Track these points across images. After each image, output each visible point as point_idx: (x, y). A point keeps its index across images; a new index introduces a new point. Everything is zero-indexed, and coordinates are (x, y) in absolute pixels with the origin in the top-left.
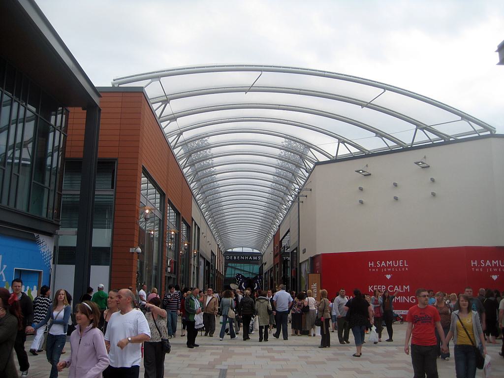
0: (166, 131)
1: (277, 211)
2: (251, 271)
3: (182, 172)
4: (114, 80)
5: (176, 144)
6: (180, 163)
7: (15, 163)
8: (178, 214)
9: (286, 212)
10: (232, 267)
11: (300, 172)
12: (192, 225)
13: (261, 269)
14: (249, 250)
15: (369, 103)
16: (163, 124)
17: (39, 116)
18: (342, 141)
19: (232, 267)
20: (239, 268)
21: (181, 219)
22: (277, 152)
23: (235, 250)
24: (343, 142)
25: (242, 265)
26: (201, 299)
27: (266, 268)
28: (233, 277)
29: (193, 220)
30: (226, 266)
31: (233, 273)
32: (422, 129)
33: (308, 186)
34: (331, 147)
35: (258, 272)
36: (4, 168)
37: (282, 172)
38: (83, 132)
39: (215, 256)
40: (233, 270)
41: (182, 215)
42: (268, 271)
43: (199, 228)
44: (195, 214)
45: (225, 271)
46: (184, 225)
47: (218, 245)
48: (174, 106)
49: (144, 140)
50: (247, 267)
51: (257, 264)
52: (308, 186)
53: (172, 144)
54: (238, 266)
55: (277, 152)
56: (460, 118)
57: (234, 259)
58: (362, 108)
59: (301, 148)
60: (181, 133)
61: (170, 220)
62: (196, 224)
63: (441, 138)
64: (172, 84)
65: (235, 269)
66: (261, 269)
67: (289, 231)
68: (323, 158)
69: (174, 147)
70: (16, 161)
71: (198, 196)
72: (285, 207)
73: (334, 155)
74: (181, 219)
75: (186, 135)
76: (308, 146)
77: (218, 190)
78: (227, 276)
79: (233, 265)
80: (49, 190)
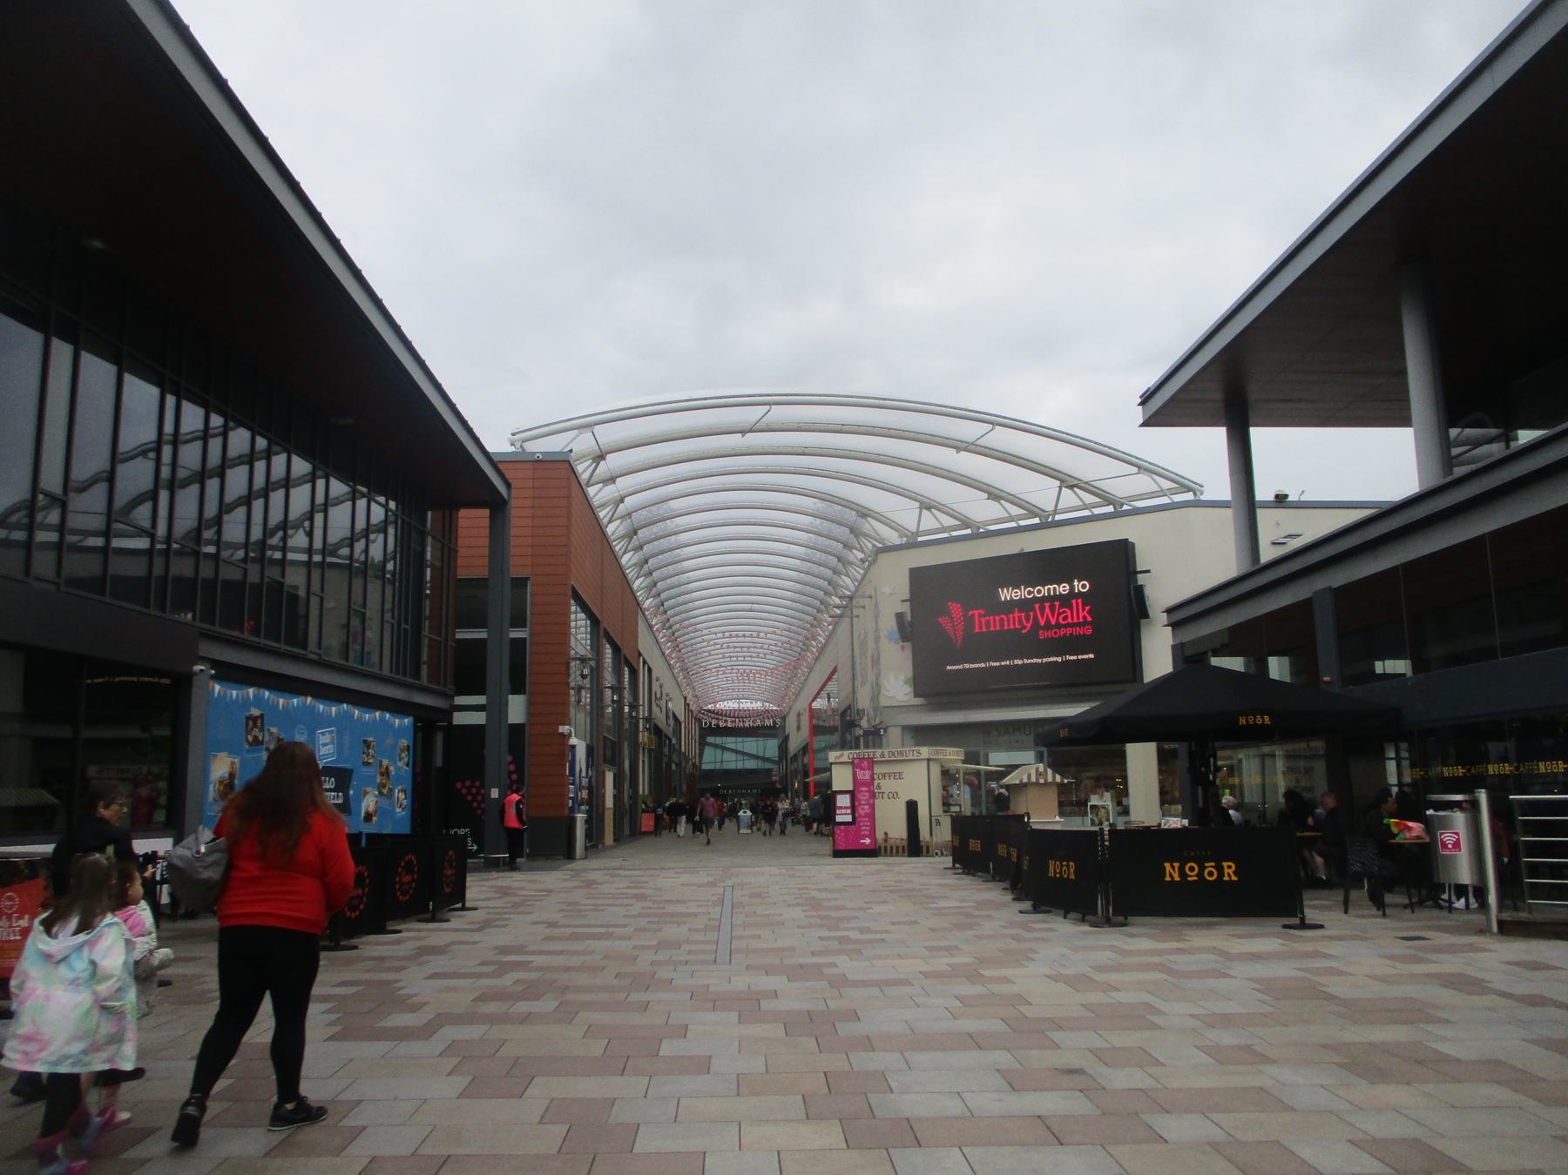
0: (596, 502)
1: (835, 572)
2: (761, 754)
3: (604, 534)
4: (513, 434)
5: (591, 476)
6: (601, 514)
7: (316, 563)
8: (595, 621)
9: (862, 572)
10: (716, 746)
11: (867, 525)
12: (639, 663)
13: (783, 747)
14: (757, 705)
15: (972, 444)
16: (591, 491)
17: (413, 522)
18: (927, 505)
19: (716, 746)
20: (733, 746)
21: (602, 633)
22: (805, 520)
23: (721, 706)
24: (929, 508)
25: (740, 739)
26: (1464, 805)
27: (794, 744)
28: (718, 767)
29: (640, 654)
30: (703, 744)
31: (719, 760)
32: (1071, 487)
33: (868, 590)
34: (907, 515)
35: (777, 754)
36: (363, 611)
37: (818, 556)
38: (486, 552)
39: (680, 724)
40: (719, 752)
41: (604, 624)
42: (799, 751)
43: (650, 670)
44: (645, 643)
45: (701, 756)
46: (608, 646)
47: (685, 698)
48: (613, 462)
49: (573, 550)
50: (750, 745)
51: (774, 736)
52: (868, 590)
53: (605, 521)
54: (730, 742)
55: (805, 520)
56: (1135, 470)
57: (715, 728)
58: (957, 453)
59: (850, 516)
60: (622, 500)
61: (579, 637)
62: (645, 662)
63: (1105, 503)
64: (609, 434)
65: (724, 749)
66: (783, 747)
67: (835, 670)
68: (893, 538)
69: (588, 482)
70: (317, 558)
71: (648, 602)
72: (861, 555)
73: (915, 530)
74: (602, 633)
75: (630, 502)
76: (864, 513)
77: (679, 555)
78: (704, 767)
79: (718, 740)
80: (322, 598)
